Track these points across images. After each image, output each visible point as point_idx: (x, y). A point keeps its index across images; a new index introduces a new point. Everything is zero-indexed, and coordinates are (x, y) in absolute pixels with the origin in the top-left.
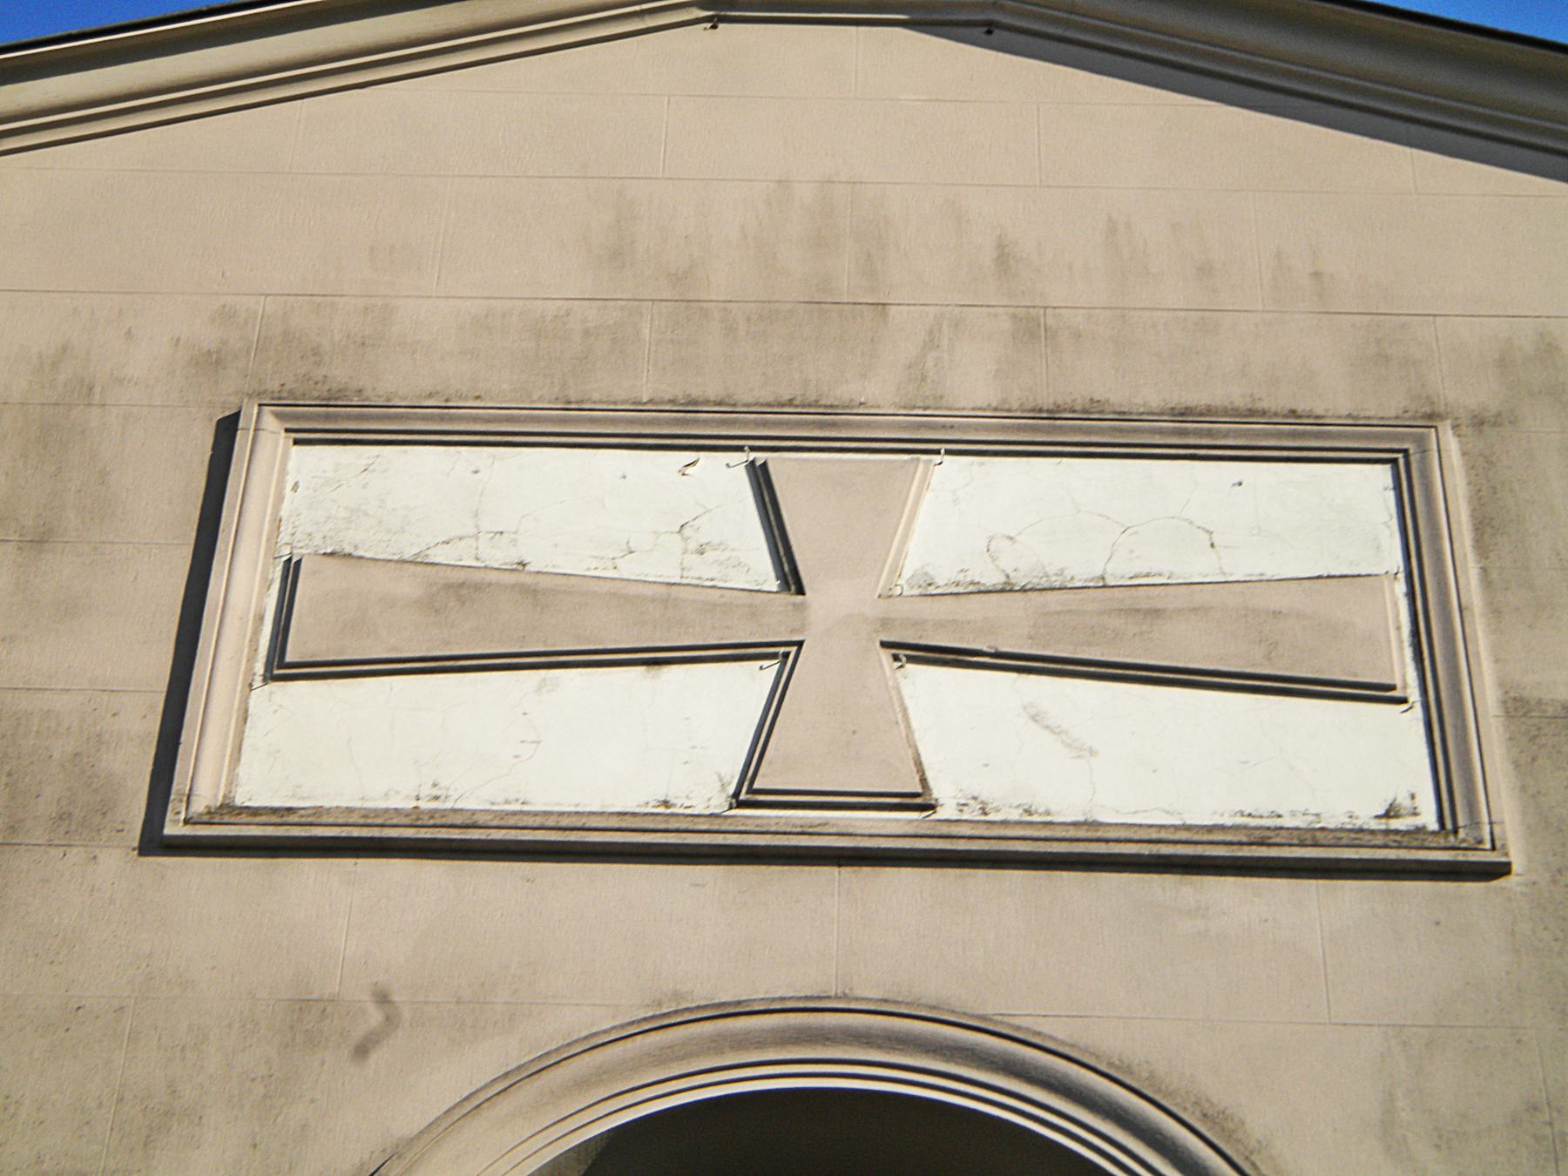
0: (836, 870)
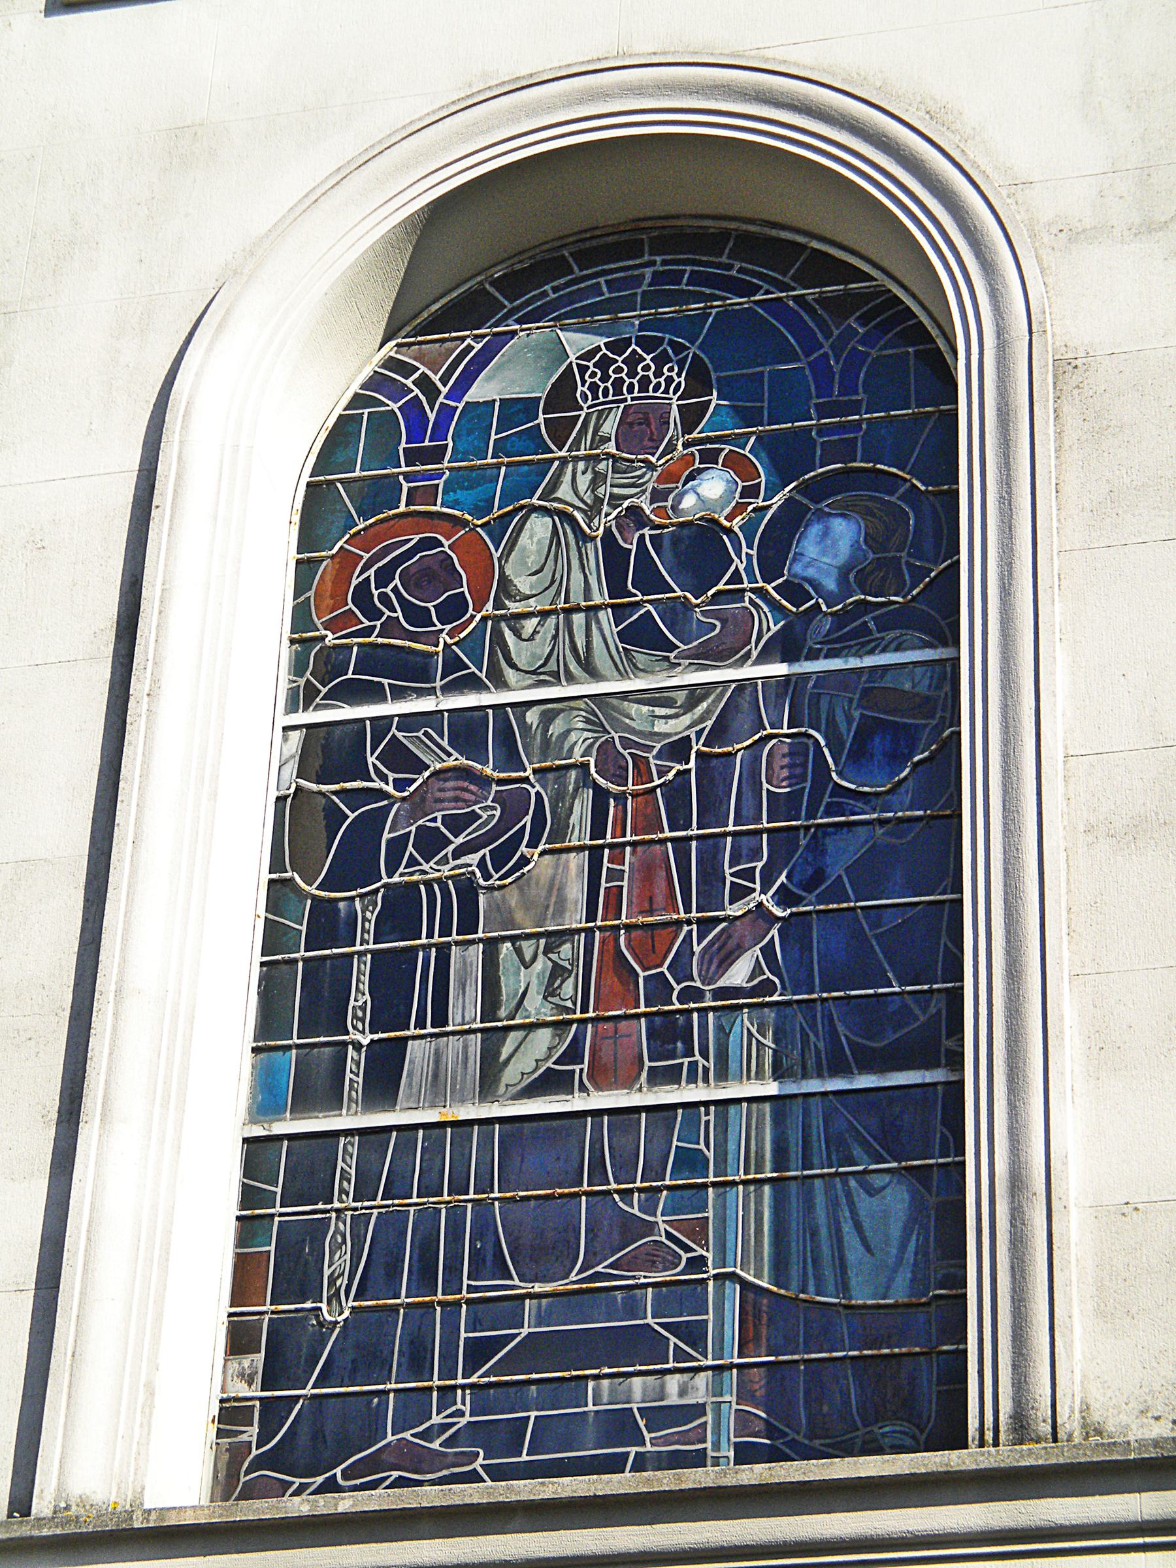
0: (1142, 1554)
